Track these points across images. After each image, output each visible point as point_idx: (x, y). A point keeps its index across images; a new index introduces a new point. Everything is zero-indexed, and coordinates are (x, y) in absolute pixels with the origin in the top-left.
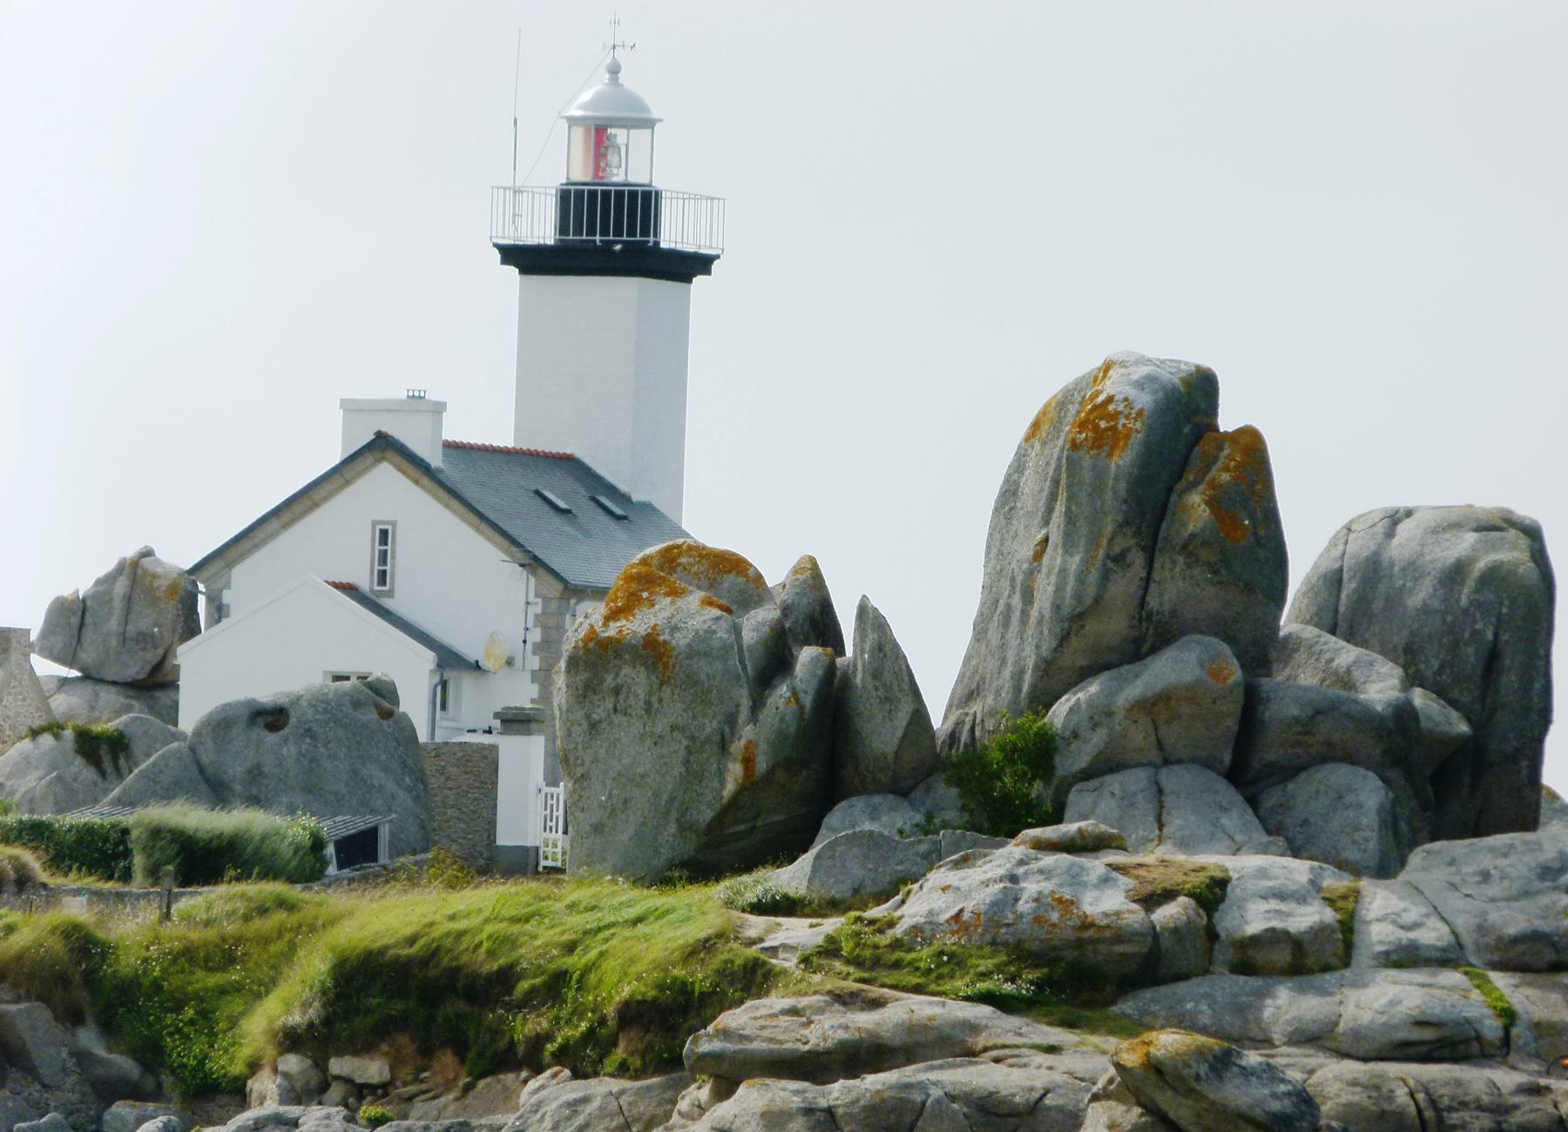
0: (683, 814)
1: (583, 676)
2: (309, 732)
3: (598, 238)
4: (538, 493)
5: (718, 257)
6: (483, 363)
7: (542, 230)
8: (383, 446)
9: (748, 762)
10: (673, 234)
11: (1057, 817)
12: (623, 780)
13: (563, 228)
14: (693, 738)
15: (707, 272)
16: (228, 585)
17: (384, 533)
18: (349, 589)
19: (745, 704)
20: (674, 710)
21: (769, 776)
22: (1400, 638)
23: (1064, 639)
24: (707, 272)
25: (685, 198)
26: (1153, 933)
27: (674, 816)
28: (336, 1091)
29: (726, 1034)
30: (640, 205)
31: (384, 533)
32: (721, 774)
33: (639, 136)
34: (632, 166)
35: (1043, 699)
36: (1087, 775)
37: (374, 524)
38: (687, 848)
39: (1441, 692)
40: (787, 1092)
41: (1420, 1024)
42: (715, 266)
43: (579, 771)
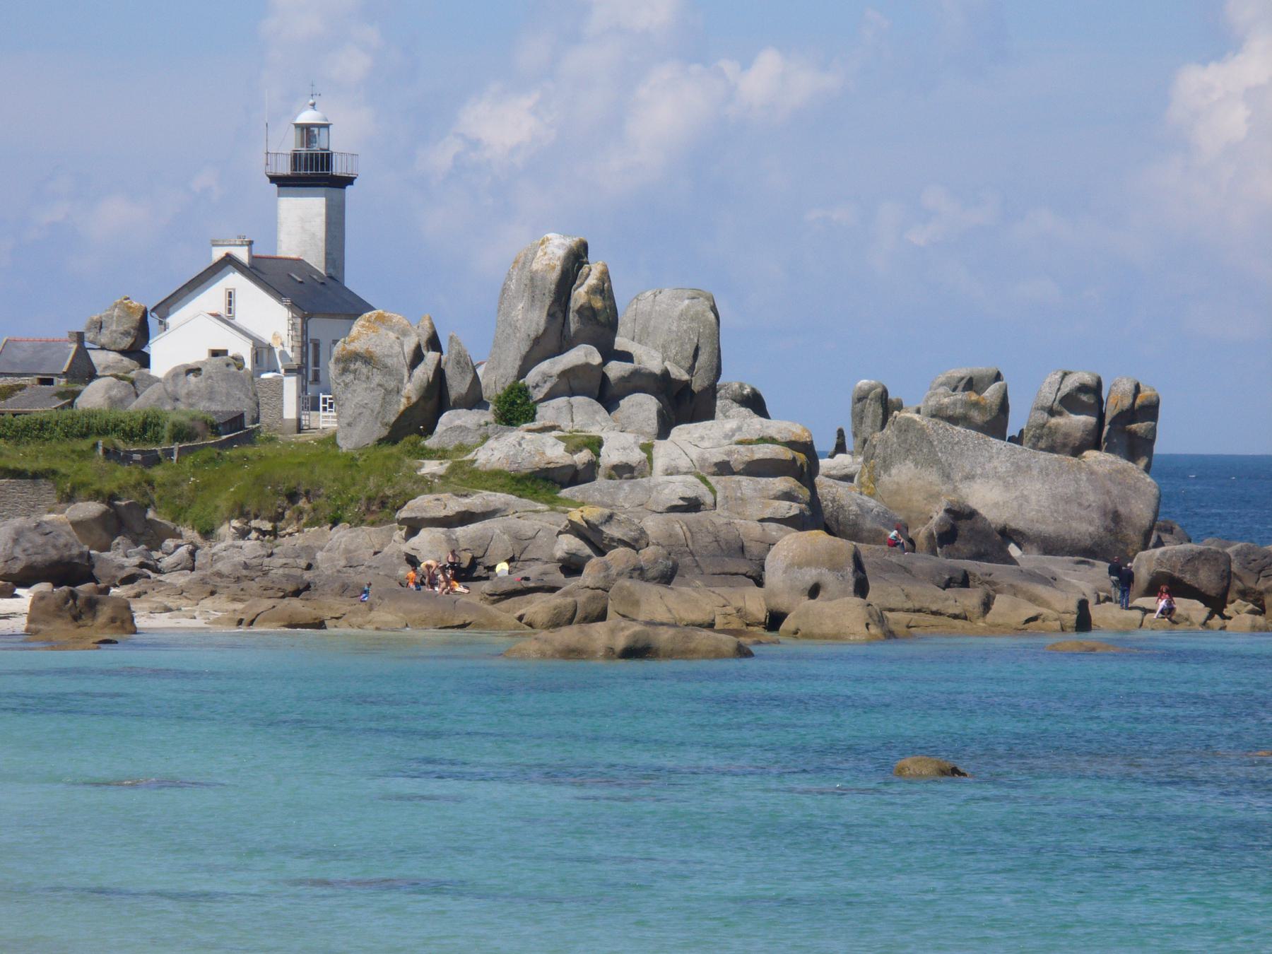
1: (341, 365)
2: (210, 377)
7: (285, 169)
9: (408, 398)
10: (338, 169)
11: (533, 419)
15: (351, 183)
18: (216, 316)
20: (377, 378)
21: (416, 404)
22: (660, 341)
23: (532, 349)
26: (573, 467)
28: (254, 535)
29: (412, 510)
30: (325, 159)
32: (398, 402)
33: (323, 131)
34: (320, 145)
35: (523, 372)
36: (542, 400)
38: (384, 432)
39: (677, 363)
40: (439, 532)
41: (682, 499)
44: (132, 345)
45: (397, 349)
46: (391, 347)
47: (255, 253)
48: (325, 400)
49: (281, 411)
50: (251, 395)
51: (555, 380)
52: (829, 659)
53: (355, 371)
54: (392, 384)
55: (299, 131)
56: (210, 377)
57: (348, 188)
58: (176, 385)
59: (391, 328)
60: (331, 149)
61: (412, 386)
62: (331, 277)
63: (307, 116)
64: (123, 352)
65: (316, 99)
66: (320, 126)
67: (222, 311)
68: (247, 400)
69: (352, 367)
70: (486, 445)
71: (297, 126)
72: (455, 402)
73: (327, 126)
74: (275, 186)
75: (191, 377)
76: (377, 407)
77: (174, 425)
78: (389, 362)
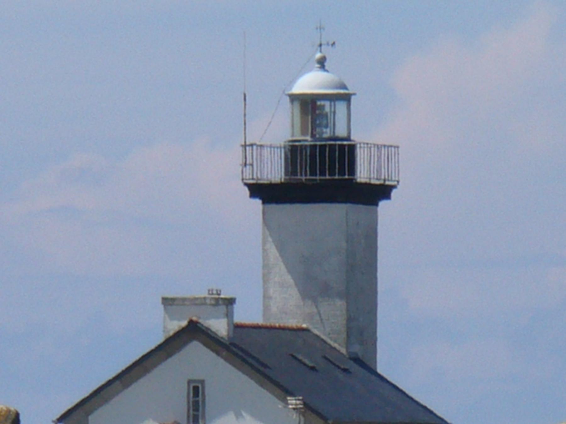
5: (394, 187)
6: (251, 271)
7: (274, 171)
8: (194, 331)
10: (363, 173)
13: (286, 174)
25: (360, 144)
30: (342, 154)
33: (341, 107)
37: (189, 382)
42: (394, 193)
51: (166, 316)
52: (364, 166)
55: (297, 105)
57: (383, 204)
60: (355, 137)
62: (357, 360)
63: (310, 82)
65: (327, 51)
70: (345, 333)
71: (294, 98)
72: (312, 287)
73: (347, 98)
74: (258, 202)
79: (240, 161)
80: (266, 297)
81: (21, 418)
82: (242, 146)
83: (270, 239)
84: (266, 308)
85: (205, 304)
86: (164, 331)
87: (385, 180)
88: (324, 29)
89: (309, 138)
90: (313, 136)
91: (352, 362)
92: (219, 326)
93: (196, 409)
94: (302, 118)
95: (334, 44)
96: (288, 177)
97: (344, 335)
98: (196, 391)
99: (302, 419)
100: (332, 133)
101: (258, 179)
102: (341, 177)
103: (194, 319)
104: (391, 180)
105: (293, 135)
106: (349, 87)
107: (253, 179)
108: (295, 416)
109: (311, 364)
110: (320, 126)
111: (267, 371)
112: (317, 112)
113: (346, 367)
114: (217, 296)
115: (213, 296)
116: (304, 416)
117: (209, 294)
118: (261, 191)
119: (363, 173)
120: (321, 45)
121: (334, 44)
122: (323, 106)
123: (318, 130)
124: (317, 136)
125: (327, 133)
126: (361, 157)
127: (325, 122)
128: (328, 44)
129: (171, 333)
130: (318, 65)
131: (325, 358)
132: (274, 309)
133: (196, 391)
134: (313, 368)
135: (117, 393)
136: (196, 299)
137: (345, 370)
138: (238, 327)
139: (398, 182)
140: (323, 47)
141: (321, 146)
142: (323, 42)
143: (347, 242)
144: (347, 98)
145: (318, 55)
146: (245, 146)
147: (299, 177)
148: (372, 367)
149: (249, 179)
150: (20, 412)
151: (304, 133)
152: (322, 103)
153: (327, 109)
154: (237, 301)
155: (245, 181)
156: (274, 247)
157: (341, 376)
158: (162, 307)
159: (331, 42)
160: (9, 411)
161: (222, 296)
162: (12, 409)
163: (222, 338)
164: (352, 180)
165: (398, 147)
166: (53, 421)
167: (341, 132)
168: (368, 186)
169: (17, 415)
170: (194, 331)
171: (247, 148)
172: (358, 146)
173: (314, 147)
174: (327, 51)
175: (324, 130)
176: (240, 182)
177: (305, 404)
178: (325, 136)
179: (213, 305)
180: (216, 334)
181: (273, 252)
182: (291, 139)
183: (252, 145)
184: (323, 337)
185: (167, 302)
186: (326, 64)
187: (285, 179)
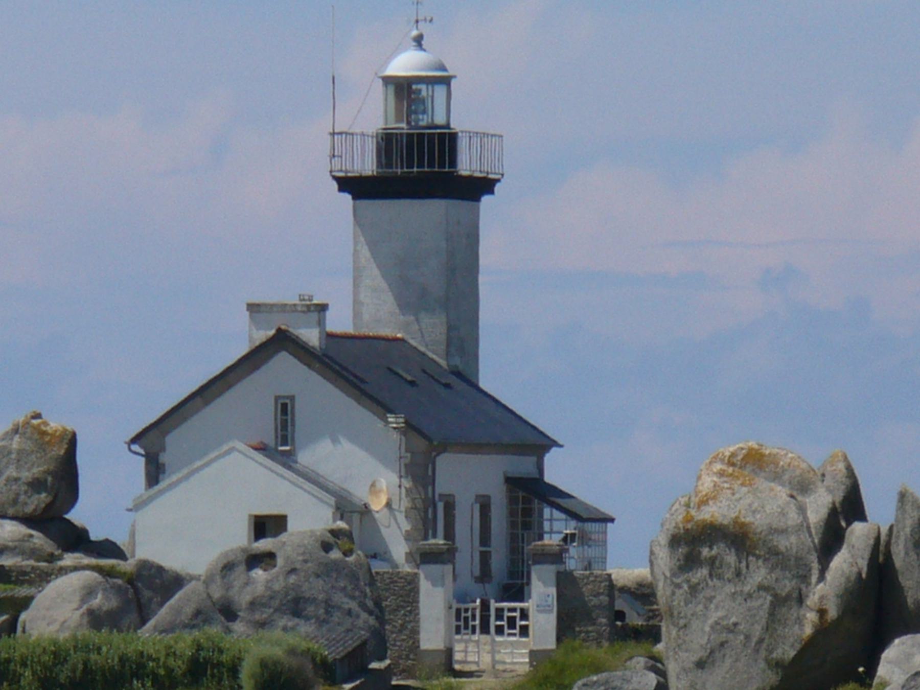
0: (771, 652)
1: (682, 550)
3: (415, 169)
4: (390, 370)
5: (498, 180)
6: (338, 272)
7: (366, 164)
8: (282, 341)
9: (822, 612)
10: (467, 165)
12: (718, 627)
13: (379, 164)
14: (775, 596)
15: (491, 191)
16: (163, 449)
17: (284, 407)
19: (815, 566)
20: (759, 574)
24: (491, 191)
25: (462, 132)
27: (763, 653)
30: (445, 143)
31: (284, 407)
32: (800, 621)
33: (440, 92)
37: (277, 398)
42: (498, 188)
43: (682, 622)
44: (49, 506)
45: (793, 517)
46: (783, 514)
47: (330, 328)
48: (499, 614)
49: (415, 632)
50: (370, 604)
53: (712, 561)
54: (787, 586)
55: (391, 89)
56: (293, 571)
57: (486, 199)
58: (228, 587)
59: (776, 477)
61: (827, 589)
62: (458, 374)
63: (406, 63)
64: (28, 520)
65: (424, 28)
66: (431, 81)
67: (270, 440)
68: (364, 615)
69: (705, 552)
71: (387, 80)
73: (446, 81)
74: (347, 197)
75: (258, 574)
76: (757, 631)
77: (263, 664)
78: (783, 543)
79: (328, 151)
80: (357, 303)
81: (78, 438)
82: (331, 134)
83: (362, 239)
84: (357, 315)
85: (296, 311)
86: (250, 341)
87: (488, 173)
88: (421, 4)
89: (404, 125)
90: (408, 123)
91: (454, 377)
92: (311, 336)
93: (284, 426)
94: (396, 103)
95: (431, 21)
96: (380, 170)
97: (443, 347)
98: (285, 409)
99: (403, 438)
100: (430, 120)
101: (346, 172)
102: (419, 170)
103: (283, 327)
104: (495, 173)
105: (386, 123)
106: (448, 66)
107: (341, 171)
108: (396, 436)
109: (409, 378)
110: (416, 113)
111: (363, 386)
112: (413, 96)
113: (448, 382)
114: (308, 303)
115: (304, 303)
116: (405, 436)
117: (301, 300)
118: (350, 185)
119: (467, 165)
120: (417, 22)
121: (431, 21)
122: (420, 91)
123: (413, 117)
124: (413, 124)
125: (424, 120)
126: (463, 145)
127: (422, 108)
128: (425, 20)
129: (257, 344)
130: (414, 44)
131: (424, 371)
132: (366, 317)
133: (285, 409)
134: (412, 383)
135: (198, 410)
136: (286, 305)
137: (447, 386)
138: (331, 336)
139: (503, 175)
140: (419, 24)
141: (418, 134)
142: (420, 18)
143: (447, 240)
144: (446, 81)
145: (415, 33)
146: (333, 134)
147: (394, 170)
148: (474, 380)
149: (338, 171)
150: (78, 433)
151: (398, 120)
152: (419, 86)
153: (424, 93)
154: (330, 306)
155: (334, 174)
156: (366, 247)
157: (443, 392)
158: (248, 313)
159: (429, 18)
160: (65, 430)
161: (315, 302)
162: (69, 428)
163: (313, 348)
164: (453, 172)
165: (502, 136)
166: (126, 443)
167: (440, 119)
168: (471, 179)
169: (74, 435)
170: (282, 341)
171: (336, 137)
172: (460, 134)
173: (410, 136)
174: (424, 28)
175: (421, 117)
176: (328, 174)
177: (406, 422)
178: (421, 123)
179: (303, 312)
180: (307, 344)
181: (365, 252)
182: (384, 127)
183: (341, 133)
184: (422, 349)
185: (253, 308)
186: (423, 42)
187: (377, 172)
